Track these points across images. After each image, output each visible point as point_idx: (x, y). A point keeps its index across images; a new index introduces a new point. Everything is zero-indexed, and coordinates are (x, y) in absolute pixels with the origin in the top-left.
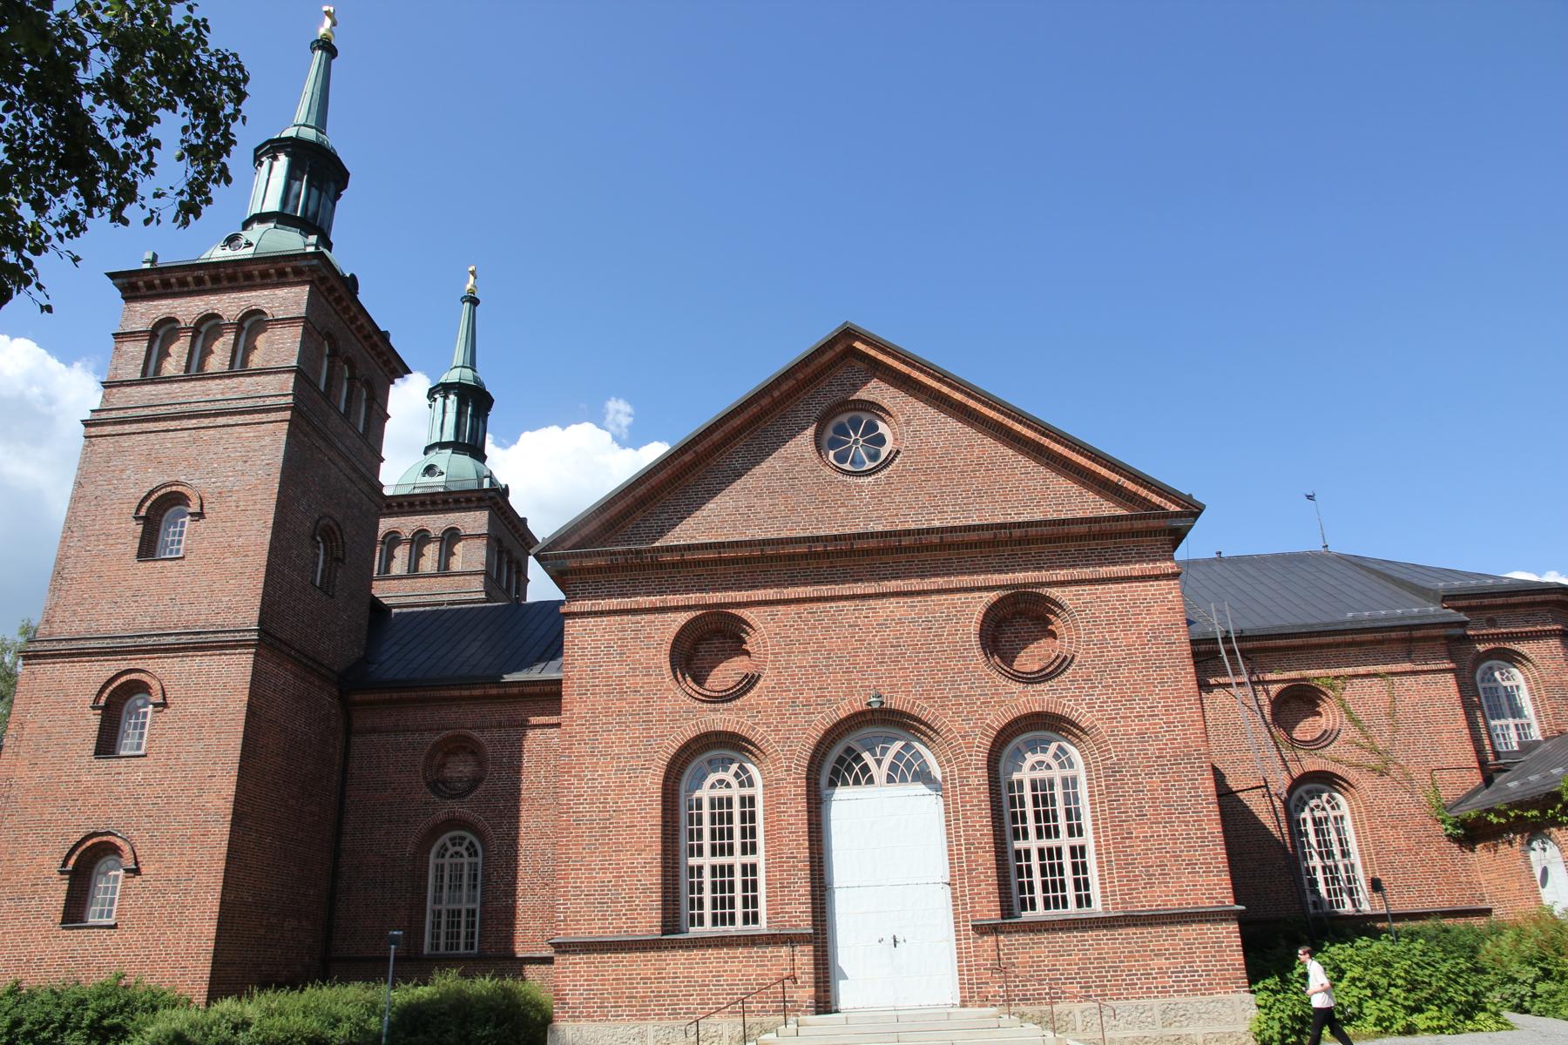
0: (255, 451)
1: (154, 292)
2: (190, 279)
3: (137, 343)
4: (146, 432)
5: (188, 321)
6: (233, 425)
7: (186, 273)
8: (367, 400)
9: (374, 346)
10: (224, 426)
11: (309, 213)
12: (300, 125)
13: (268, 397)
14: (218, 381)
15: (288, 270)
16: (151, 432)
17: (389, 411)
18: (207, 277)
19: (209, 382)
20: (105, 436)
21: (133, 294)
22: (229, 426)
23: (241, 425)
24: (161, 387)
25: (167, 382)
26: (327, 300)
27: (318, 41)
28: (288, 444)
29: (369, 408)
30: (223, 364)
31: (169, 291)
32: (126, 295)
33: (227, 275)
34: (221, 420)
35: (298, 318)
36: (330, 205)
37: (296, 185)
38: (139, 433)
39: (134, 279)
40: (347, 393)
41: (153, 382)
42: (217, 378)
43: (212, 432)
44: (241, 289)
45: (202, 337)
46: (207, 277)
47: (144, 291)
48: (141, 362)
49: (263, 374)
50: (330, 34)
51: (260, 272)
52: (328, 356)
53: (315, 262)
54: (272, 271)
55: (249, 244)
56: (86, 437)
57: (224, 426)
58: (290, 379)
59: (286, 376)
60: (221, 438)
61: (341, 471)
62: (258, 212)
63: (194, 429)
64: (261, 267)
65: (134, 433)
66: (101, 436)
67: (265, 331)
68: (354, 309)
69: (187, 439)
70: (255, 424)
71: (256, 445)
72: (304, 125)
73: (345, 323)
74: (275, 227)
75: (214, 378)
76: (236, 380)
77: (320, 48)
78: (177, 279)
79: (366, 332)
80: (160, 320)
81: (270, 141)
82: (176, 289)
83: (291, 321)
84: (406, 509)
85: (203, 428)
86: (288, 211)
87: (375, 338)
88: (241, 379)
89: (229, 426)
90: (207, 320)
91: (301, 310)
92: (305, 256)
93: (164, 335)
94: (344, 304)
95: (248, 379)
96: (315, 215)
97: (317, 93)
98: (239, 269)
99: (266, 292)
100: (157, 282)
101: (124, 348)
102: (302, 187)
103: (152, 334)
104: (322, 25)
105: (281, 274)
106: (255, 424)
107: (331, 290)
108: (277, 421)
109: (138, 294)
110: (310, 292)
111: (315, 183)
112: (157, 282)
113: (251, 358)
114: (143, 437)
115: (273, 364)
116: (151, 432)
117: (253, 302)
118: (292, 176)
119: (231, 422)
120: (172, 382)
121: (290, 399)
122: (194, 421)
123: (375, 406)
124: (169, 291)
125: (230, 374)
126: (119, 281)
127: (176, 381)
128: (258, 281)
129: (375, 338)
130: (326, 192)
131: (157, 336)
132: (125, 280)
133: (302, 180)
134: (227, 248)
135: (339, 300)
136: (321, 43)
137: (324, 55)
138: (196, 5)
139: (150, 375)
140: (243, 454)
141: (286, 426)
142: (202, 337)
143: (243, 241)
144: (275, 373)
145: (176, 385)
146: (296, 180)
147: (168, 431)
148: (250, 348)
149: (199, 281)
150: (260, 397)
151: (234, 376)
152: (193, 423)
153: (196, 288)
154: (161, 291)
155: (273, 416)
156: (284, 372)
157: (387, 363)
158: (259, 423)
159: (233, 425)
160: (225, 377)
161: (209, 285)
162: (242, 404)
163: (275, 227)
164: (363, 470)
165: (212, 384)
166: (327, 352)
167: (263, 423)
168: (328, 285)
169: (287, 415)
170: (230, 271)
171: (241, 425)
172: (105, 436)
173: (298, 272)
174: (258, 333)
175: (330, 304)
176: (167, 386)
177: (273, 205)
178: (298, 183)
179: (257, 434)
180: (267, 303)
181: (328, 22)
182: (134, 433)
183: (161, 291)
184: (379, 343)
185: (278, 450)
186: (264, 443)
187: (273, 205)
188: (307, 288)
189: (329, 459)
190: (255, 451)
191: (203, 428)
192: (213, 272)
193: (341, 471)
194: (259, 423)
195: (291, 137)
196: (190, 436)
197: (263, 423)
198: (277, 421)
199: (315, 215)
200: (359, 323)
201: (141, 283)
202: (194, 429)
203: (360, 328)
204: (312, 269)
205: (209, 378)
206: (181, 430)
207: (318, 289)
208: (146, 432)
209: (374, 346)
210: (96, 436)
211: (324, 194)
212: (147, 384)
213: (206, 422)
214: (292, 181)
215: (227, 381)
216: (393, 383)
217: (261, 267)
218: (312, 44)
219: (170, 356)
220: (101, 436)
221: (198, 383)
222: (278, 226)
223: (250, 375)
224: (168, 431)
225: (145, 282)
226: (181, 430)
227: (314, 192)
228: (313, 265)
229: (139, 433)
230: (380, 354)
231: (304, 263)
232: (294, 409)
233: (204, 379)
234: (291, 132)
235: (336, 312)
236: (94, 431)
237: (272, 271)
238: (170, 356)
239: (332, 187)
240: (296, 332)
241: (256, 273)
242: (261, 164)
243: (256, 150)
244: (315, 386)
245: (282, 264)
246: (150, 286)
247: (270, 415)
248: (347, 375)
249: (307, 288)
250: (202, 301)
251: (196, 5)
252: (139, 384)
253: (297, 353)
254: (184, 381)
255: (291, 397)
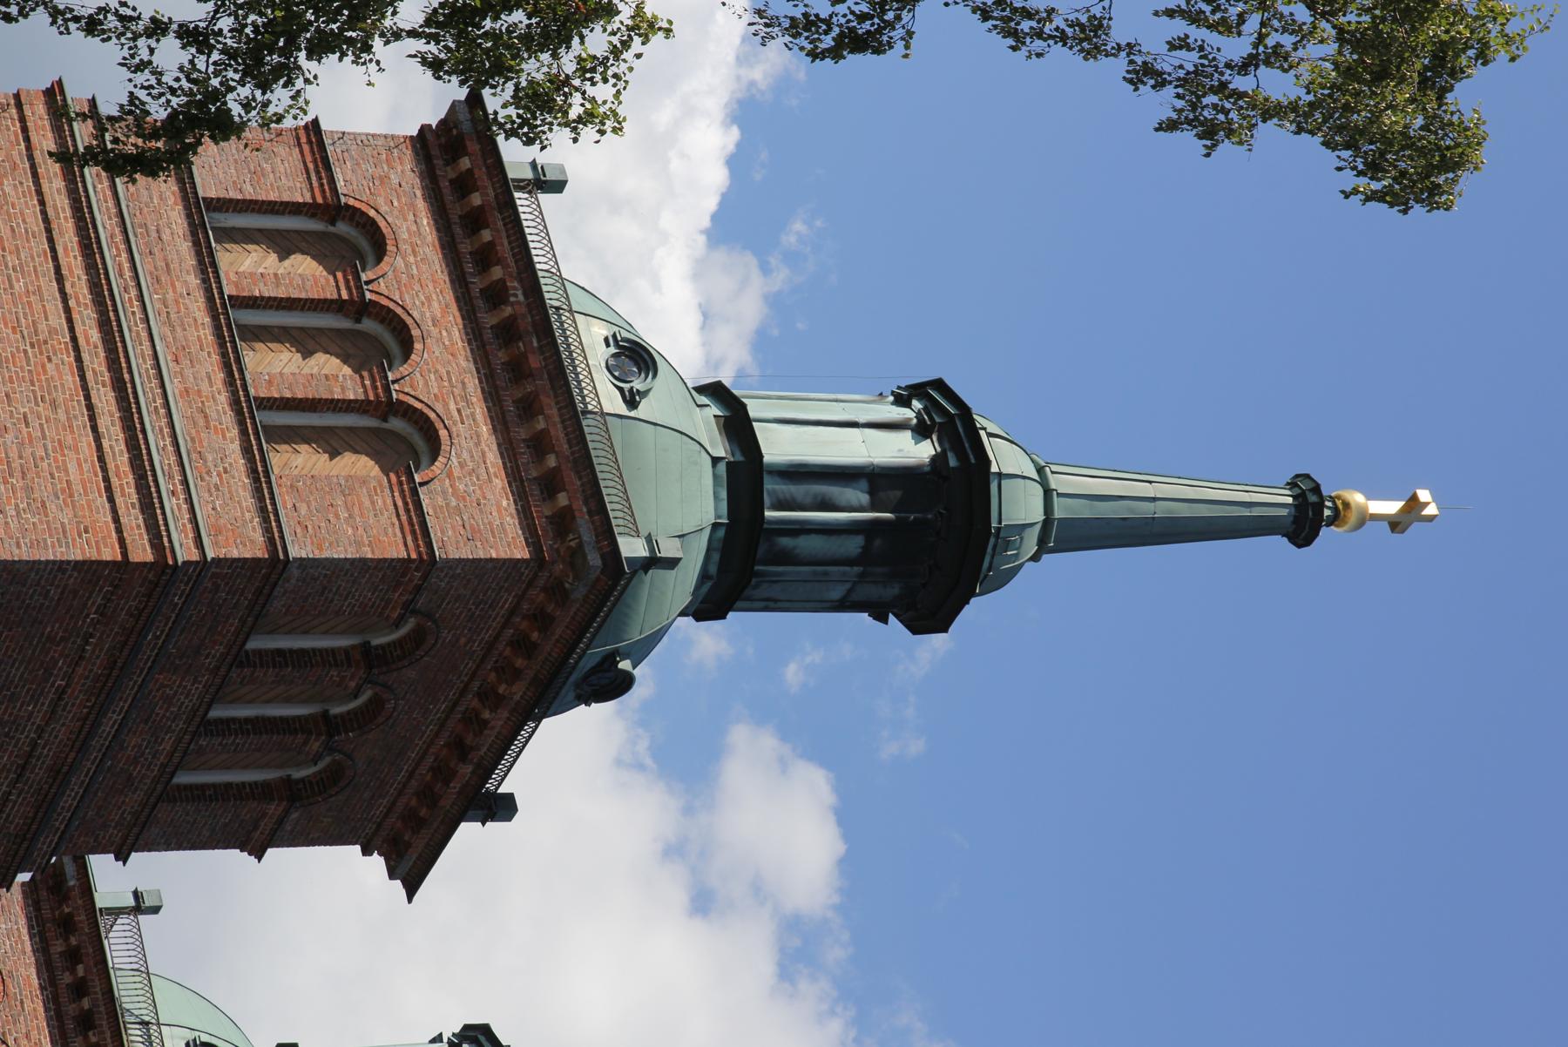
0: (29, 490)
1: (449, 197)
2: (497, 273)
3: (302, 178)
4: (49, 230)
5: (382, 286)
6: (95, 428)
7: (511, 261)
8: (288, 781)
9: (443, 773)
10: (90, 407)
11: (785, 542)
12: (1044, 482)
13: (189, 501)
14: (220, 376)
15: (562, 499)
16: (51, 240)
17: (271, 853)
18: (508, 311)
19: (215, 358)
20: (27, 139)
21: (435, 152)
22: (92, 418)
23: (99, 447)
24: (185, 247)
25: (201, 262)
26: (513, 612)
27: (1316, 489)
28: (61, 566)
29: (263, 791)
30: (270, 382)
31: (458, 230)
32: (429, 136)
33: (524, 356)
34: (105, 399)
35: (429, 545)
36: (837, 593)
37: (859, 495)
38: (44, 213)
39: (473, 146)
40: (283, 719)
41: (196, 229)
42: (230, 374)
43: (71, 380)
44: (492, 395)
45: (345, 324)
46: (508, 311)
47: (447, 174)
48: (249, 192)
49: (256, 480)
50: (1353, 518)
51: (544, 432)
52: (366, 646)
53: (594, 559)
54: (552, 461)
55: (631, 400)
56: (17, 96)
57: (90, 407)
58: (248, 543)
59: (259, 537)
60: (54, 405)
61: (40, 731)
62: (752, 414)
63: (74, 339)
64: (558, 434)
65: (42, 203)
66: (25, 130)
67: (386, 471)
68: (518, 691)
69: (42, 326)
70: (106, 479)
71: (43, 490)
72: (1048, 492)
73: (473, 676)
74: (715, 461)
75: (227, 366)
76: (229, 418)
77: (1300, 497)
78: (491, 244)
79: (469, 740)
80: (373, 222)
81: (965, 412)
82: (465, 247)
83: (418, 525)
84: (71, 1009)
85: (79, 359)
86: (770, 485)
87: (466, 770)
88: (234, 432)
89: (92, 418)
90: (393, 330)
91: (451, 543)
92: (606, 534)
93: (341, 239)
94: (519, 662)
95: (235, 447)
96: (787, 558)
97: (1161, 510)
98: (543, 382)
99: (493, 457)
100: (476, 199)
101: (281, 150)
102: (853, 508)
103: (332, 209)
104: (1369, 498)
105: (550, 485)
106: (106, 479)
107: (542, 620)
108: (119, 530)
109: (438, 162)
110: (514, 563)
111: (878, 542)
112: (476, 199)
113: (303, 448)
114: (37, 226)
115: (285, 500)
116: (51, 240)
117: (460, 429)
118: (876, 479)
119: (103, 423)
120: (204, 271)
121: (185, 551)
122: (95, 335)
123: (274, 809)
124: (458, 230)
125: (245, 405)
126: (464, 115)
127: (206, 281)
128: (522, 433)
129: (466, 770)
130: (862, 575)
131: (333, 222)
132: (466, 127)
133: (873, 507)
134: (613, 350)
135: (523, 645)
136: (1313, 498)
137: (1284, 512)
138: (597, 142)
139: (211, 219)
140: (16, 464)
141: (110, 553)
142: (345, 324)
143: (638, 385)
144: (263, 510)
145: (194, 281)
146: (872, 493)
147: (60, 278)
148: (333, 443)
149: (496, 295)
150: (185, 482)
151: (239, 412)
152: (90, 334)
153: (476, 291)
154: (456, 211)
155: (133, 520)
156: (267, 530)
157: (414, 821)
158: (109, 489)
159: (95, 428)
160: (235, 393)
161: (489, 320)
162: (157, 442)
163: (715, 461)
164: (68, 800)
165: (210, 364)
166: (376, 642)
167: (111, 500)
168: (550, 608)
169: (142, 552)
170: (535, 362)
171: (99, 447)
172: (27, 139)
173: (562, 523)
174: (375, 455)
175: (505, 626)
176: (191, 261)
177: (778, 446)
178: (864, 498)
179: (77, 488)
180: (462, 465)
181: (1392, 507)
182: (42, 203)
183: (456, 211)
184: (456, 786)
185: (38, 543)
186: (52, 507)
187: (778, 446)
188: (521, 552)
189: (61, 693)
190: (29, 490)
191: (79, 359)
192: (526, 323)
193: (40, 731)
194: (109, 489)
195: (986, 462)
196: (52, 331)
197: (111, 500)
198: (119, 530)
199: (787, 558)
200: (486, 715)
201: (465, 163)
202: (74, 339)
203: (474, 722)
204: (575, 557)
205: (224, 355)
206: (67, 310)
207: (530, 584)
208: (49, 230)
209: (443, 773)
210: (22, 119)
211: (857, 569)
212: (189, 216)
213: (96, 363)
214: (864, 484)
215: (223, 398)
216: (366, 852)
217: (558, 434)
218: (1307, 476)
219: (281, 259)
220: (25, 130)
221: (207, 334)
222: (722, 467)
223: (247, 451)
224: (60, 278)
225: (470, 171)
226: (67, 310)
227: (854, 545)
228: (584, 557)
229: (44, 213)
230: (428, 796)
231: (587, 536)
232: (163, 571)
233: (221, 343)
234: (1004, 457)
235: (490, 646)
236: (38, 113)
237: (552, 461)
238: (281, 259)
239: (892, 591)
240: (392, 545)
241: (541, 424)
242: (901, 400)
243: (939, 385)
244: (257, 619)
245: (571, 479)
246: (464, 185)
247: (136, 512)
248: (337, 710)
249: (521, 552)
250: (445, 312)
251: (597, 142)
252: (185, 198)
253: (326, 554)
254: (210, 299)
255: (195, 556)
